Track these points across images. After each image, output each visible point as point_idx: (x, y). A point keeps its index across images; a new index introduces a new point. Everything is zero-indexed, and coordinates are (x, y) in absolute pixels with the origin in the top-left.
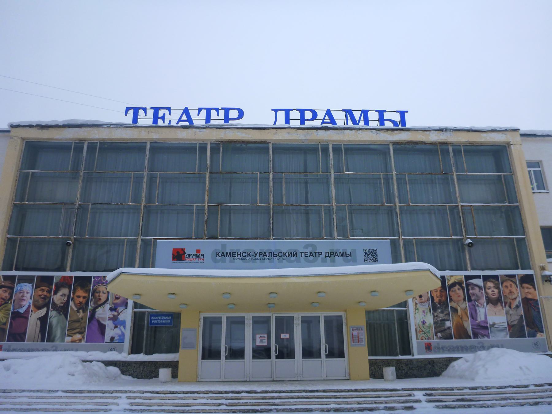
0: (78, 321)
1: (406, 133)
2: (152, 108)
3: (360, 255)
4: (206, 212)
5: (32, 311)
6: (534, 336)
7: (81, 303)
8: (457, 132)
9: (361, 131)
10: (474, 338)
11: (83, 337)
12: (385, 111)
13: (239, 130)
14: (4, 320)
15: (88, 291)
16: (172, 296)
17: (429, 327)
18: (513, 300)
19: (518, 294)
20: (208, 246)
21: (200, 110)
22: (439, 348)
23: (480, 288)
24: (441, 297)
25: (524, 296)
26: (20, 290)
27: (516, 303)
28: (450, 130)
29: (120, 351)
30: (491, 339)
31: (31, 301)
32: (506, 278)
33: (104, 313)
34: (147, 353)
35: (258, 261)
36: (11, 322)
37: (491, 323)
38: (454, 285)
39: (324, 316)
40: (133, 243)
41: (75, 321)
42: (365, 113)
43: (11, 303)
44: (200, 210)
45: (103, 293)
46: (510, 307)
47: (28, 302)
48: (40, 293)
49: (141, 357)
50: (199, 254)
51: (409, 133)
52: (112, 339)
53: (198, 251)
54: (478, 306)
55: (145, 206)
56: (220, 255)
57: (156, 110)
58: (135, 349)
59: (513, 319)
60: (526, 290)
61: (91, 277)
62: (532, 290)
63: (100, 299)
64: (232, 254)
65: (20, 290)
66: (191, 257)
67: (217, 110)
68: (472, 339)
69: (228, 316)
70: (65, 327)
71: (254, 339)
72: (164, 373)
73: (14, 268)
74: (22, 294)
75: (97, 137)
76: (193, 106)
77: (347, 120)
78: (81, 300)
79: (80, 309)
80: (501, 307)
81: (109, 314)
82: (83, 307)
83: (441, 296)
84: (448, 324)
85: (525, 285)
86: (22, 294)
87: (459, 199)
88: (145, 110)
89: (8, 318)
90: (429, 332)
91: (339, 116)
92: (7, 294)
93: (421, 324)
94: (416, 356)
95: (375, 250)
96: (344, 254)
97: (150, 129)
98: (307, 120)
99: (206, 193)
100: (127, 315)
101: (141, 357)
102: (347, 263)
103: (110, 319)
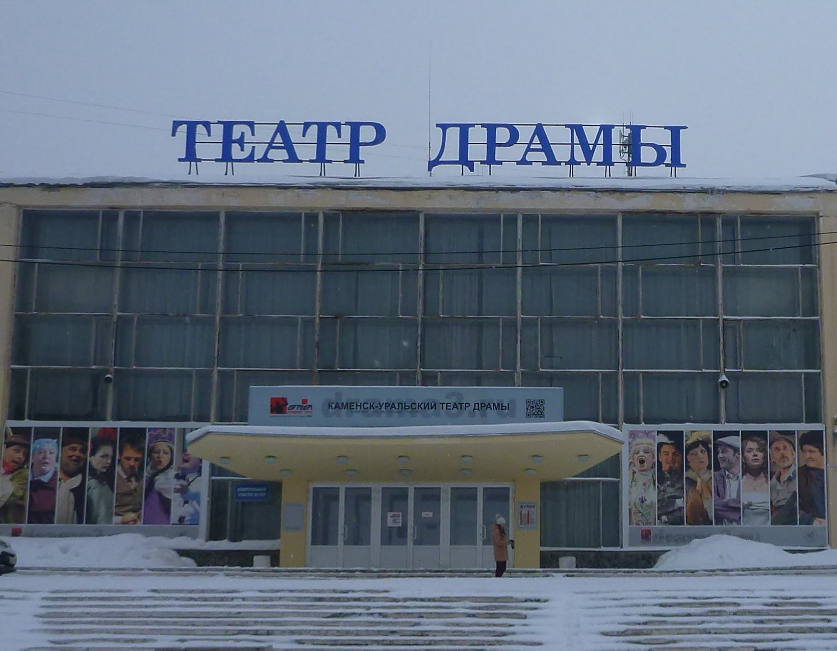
0: (129, 493)
1: (646, 196)
2: (219, 122)
3: (521, 408)
4: (317, 328)
5: (60, 480)
6: (809, 522)
7: (132, 467)
8: (731, 195)
9: (570, 194)
10: (717, 524)
11: (139, 517)
12: (644, 127)
13: (369, 192)
14: (20, 493)
15: (141, 450)
16: (271, 459)
17: (651, 506)
18: (785, 469)
19: (793, 459)
20: (318, 393)
21: (307, 125)
22: (661, 538)
23: (736, 450)
24: (674, 463)
25: (802, 464)
26: (40, 449)
27: (790, 473)
28: (719, 191)
29: (194, 536)
30: (742, 525)
31: (58, 465)
32: (779, 435)
33: (167, 482)
34: (233, 539)
35: (384, 415)
36: (31, 497)
37: (746, 503)
38: (696, 444)
39: (484, 489)
40: (204, 377)
41: (125, 494)
42: (606, 130)
43: (28, 468)
44: (308, 323)
45: (165, 453)
46: (778, 479)
47: (52, 467)
48: (71, 453)
49: (224, 545)
50: (305, 406)
51: (651, 197)
52: (181, 520)
53: (305, 401)
54: (728, 477)
55: (222, 319)
56: (333, 406)
57: (228, 127)
58: (215, 533)
59: (781, 497)
60: (808, 455)
61: (145, 429)
62: (817, 454)
63: (161, 462)
64: (349, 406)
65: (40, 449)
66: (295, 409)
67: (338, 126)
68: (714, 526)
69: (348, 486)
70: (111, 502)
71: (384, 519)
72: (260, 562)
73: (26, 415)
74: (42, 455)
75: (139, 203)
76: (294, 117)
77: (572, 144)
78: (132, 463)
79: (132, 476)
80: (764, 479)
81: (176, 484)
82: (135, 473)
83: (673, 461)
84: (679, 503)
85: (806, 447)
86: (42, 455)
87: (720, 310)
88: (207, 125)
89: (25, 490)
90: (649, 514)
91: (558, 137)
92: (20, 455)
93: (638, 501)
94: (627, 548)
95: (542, 402)
96: (499, 407)
97: (225, 190)
98: (500, 145)
99: (318, 298)
100: (201, 485)
101: (224, 545)
102: (502, 420)
103: (176, 491)
